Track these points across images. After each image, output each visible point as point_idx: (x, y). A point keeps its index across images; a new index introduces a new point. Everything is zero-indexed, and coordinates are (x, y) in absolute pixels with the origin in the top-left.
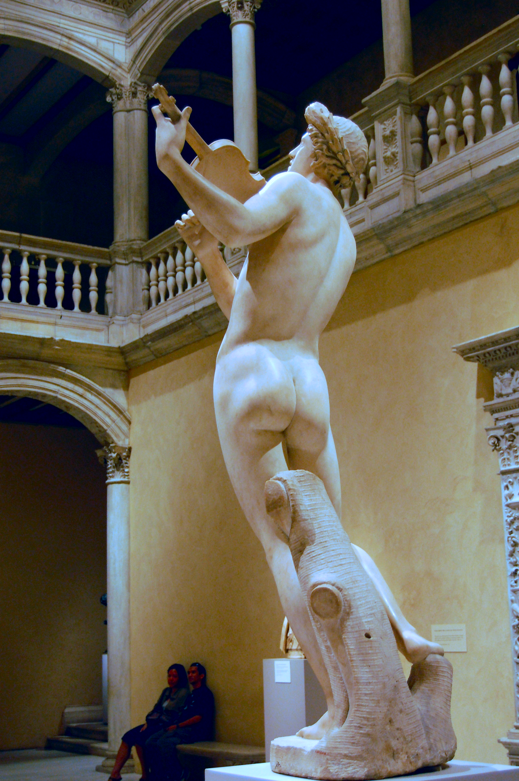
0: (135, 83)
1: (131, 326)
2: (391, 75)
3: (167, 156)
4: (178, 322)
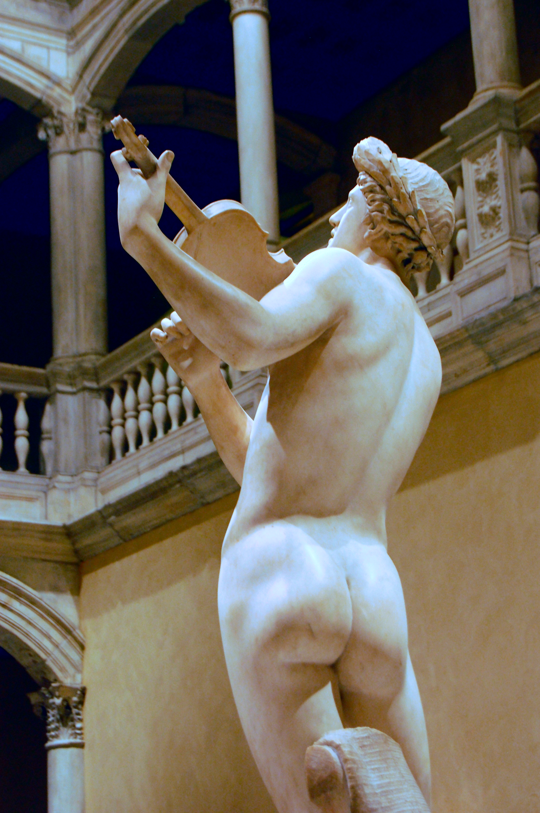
0: (83, 110)
1: (83, 491)
2: (485, 86)
3: (136, 230)
4: (158, 483)
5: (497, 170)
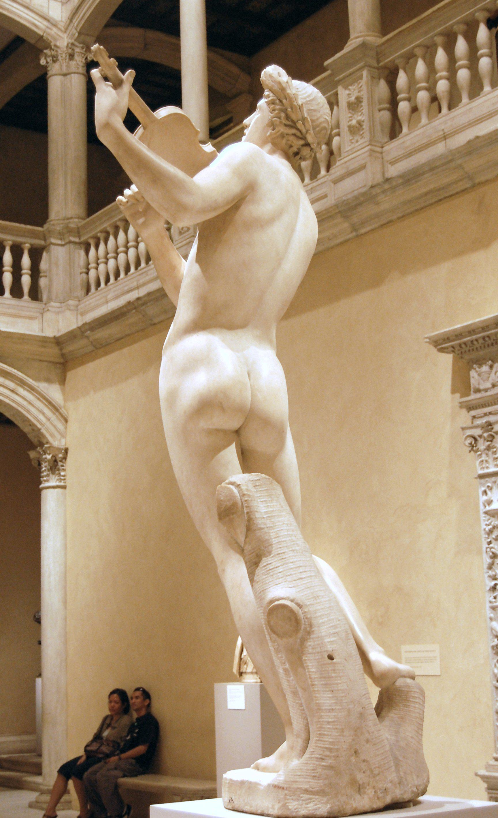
0: (72, 44)
1: (68, 313)
2: (356, 35)
3: (107, 125)
5: (363, 95)
